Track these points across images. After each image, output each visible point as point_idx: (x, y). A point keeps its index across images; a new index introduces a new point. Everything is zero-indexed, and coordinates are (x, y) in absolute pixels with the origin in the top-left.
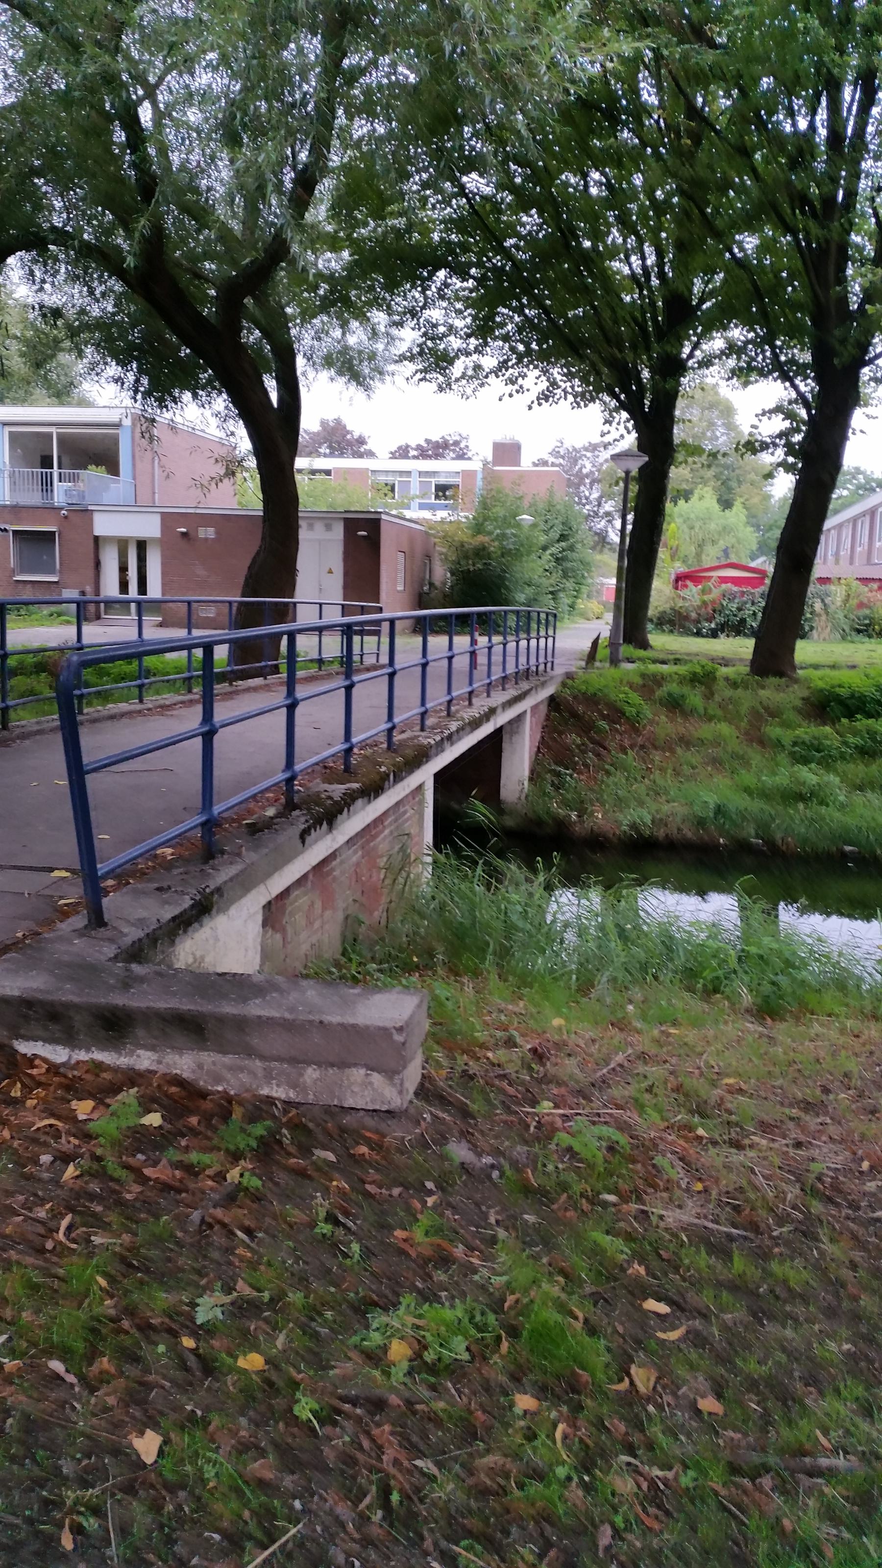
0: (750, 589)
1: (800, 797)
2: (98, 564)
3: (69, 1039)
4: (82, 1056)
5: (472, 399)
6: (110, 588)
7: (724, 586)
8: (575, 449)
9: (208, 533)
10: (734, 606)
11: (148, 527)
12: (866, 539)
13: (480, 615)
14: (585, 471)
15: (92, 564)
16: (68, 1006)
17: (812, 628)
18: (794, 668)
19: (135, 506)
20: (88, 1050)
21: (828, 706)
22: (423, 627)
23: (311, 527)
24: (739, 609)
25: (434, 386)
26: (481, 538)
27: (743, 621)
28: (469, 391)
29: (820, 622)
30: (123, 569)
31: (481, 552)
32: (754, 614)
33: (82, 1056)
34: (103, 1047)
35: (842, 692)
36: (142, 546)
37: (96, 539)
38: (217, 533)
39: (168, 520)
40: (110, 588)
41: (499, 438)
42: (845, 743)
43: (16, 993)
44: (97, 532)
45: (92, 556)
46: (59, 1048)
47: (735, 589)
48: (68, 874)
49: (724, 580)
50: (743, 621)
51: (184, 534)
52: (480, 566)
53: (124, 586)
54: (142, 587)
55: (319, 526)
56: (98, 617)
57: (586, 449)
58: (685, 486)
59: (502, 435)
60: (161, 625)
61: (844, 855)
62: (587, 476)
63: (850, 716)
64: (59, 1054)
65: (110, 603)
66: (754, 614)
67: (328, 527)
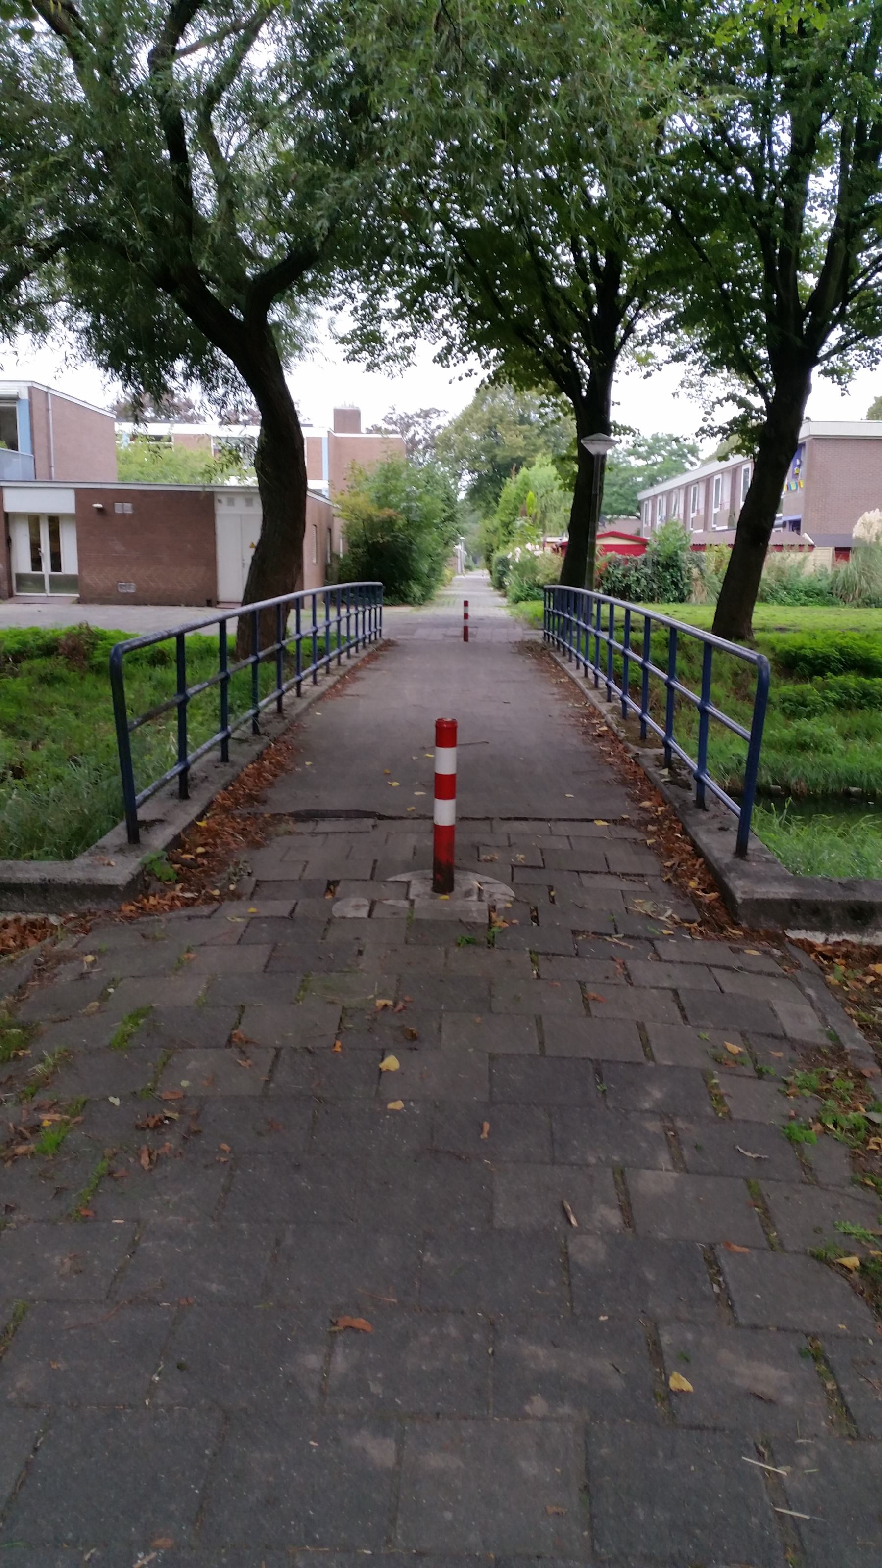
0: (632, 556)
1: (803, 747)
2: (9, 541)
3: (826, 927)
4: (834, 938)
5: (398, 378)
6: (22, 563)
7: (609, 554)
8: (408, 416)
9: (125, 508)
10: (619, 573)
11: (62, 502)
12: (702, 506)
13: (367, 586)
14: (417, 438)
15: (3, 541)
16: (826, 903)
17: (690, 592)
18: (750, 631)
19: (41, 478)
20: (839, 934)
21: (796, 664)
22: (332, 599)
23: (231, 502)
24: (624, 576)
25: (363, 365)
26: (388, 512)
27: (628, 587)
28: (396, 371)
29: (697, 587)
30: (35, 546)
31: (388, 525)
32: (638, 580)
33: (834, 938)
34: (852, 931)
35: (808, 652)
36: (54, 521)
37: (7, 515)
38: (134, 508)
39: (83, 496)
40: (22, 563)
41: (339, 406)
42: (826, 698)
43: (788, 897)
44: (8, 508)
45: (3, 533)
46: (818, 934)
47: (619, 556)
48: (605, 823)
49: (608, 548)
50: (628, 587)
51: (99, 509)
52: (388, 538)
53: (36, 563)
54: (56, 564)
55: (240, 502)
56: (11, 595)
57: (419, 416)
58: (520, 454)
59: (345, 402)
60: (79, 601)
61: (848, 794)
62: (420, 441)
63: (821, 674)
64: (818, 938)
65: (22, 579)
66: (638, 580)
67: (249, 502)
